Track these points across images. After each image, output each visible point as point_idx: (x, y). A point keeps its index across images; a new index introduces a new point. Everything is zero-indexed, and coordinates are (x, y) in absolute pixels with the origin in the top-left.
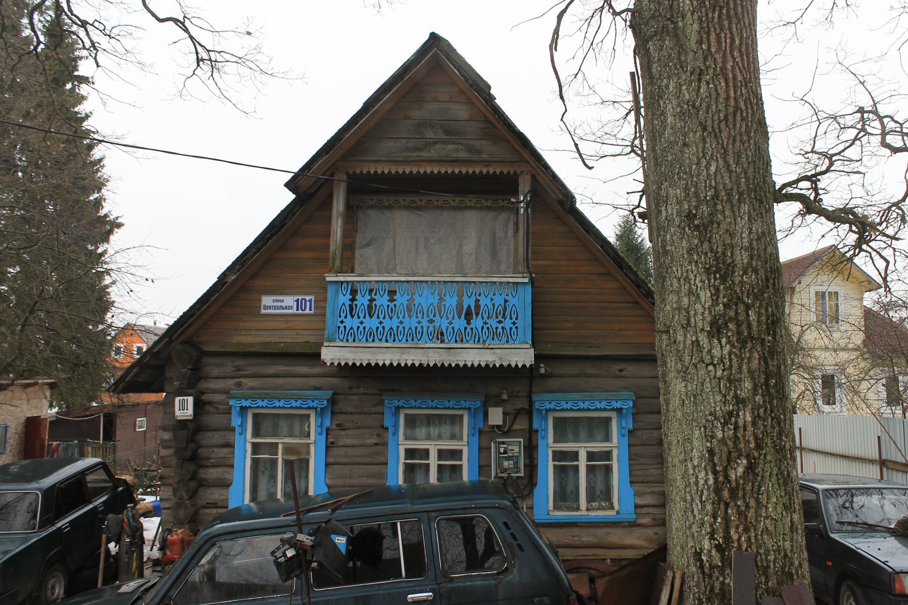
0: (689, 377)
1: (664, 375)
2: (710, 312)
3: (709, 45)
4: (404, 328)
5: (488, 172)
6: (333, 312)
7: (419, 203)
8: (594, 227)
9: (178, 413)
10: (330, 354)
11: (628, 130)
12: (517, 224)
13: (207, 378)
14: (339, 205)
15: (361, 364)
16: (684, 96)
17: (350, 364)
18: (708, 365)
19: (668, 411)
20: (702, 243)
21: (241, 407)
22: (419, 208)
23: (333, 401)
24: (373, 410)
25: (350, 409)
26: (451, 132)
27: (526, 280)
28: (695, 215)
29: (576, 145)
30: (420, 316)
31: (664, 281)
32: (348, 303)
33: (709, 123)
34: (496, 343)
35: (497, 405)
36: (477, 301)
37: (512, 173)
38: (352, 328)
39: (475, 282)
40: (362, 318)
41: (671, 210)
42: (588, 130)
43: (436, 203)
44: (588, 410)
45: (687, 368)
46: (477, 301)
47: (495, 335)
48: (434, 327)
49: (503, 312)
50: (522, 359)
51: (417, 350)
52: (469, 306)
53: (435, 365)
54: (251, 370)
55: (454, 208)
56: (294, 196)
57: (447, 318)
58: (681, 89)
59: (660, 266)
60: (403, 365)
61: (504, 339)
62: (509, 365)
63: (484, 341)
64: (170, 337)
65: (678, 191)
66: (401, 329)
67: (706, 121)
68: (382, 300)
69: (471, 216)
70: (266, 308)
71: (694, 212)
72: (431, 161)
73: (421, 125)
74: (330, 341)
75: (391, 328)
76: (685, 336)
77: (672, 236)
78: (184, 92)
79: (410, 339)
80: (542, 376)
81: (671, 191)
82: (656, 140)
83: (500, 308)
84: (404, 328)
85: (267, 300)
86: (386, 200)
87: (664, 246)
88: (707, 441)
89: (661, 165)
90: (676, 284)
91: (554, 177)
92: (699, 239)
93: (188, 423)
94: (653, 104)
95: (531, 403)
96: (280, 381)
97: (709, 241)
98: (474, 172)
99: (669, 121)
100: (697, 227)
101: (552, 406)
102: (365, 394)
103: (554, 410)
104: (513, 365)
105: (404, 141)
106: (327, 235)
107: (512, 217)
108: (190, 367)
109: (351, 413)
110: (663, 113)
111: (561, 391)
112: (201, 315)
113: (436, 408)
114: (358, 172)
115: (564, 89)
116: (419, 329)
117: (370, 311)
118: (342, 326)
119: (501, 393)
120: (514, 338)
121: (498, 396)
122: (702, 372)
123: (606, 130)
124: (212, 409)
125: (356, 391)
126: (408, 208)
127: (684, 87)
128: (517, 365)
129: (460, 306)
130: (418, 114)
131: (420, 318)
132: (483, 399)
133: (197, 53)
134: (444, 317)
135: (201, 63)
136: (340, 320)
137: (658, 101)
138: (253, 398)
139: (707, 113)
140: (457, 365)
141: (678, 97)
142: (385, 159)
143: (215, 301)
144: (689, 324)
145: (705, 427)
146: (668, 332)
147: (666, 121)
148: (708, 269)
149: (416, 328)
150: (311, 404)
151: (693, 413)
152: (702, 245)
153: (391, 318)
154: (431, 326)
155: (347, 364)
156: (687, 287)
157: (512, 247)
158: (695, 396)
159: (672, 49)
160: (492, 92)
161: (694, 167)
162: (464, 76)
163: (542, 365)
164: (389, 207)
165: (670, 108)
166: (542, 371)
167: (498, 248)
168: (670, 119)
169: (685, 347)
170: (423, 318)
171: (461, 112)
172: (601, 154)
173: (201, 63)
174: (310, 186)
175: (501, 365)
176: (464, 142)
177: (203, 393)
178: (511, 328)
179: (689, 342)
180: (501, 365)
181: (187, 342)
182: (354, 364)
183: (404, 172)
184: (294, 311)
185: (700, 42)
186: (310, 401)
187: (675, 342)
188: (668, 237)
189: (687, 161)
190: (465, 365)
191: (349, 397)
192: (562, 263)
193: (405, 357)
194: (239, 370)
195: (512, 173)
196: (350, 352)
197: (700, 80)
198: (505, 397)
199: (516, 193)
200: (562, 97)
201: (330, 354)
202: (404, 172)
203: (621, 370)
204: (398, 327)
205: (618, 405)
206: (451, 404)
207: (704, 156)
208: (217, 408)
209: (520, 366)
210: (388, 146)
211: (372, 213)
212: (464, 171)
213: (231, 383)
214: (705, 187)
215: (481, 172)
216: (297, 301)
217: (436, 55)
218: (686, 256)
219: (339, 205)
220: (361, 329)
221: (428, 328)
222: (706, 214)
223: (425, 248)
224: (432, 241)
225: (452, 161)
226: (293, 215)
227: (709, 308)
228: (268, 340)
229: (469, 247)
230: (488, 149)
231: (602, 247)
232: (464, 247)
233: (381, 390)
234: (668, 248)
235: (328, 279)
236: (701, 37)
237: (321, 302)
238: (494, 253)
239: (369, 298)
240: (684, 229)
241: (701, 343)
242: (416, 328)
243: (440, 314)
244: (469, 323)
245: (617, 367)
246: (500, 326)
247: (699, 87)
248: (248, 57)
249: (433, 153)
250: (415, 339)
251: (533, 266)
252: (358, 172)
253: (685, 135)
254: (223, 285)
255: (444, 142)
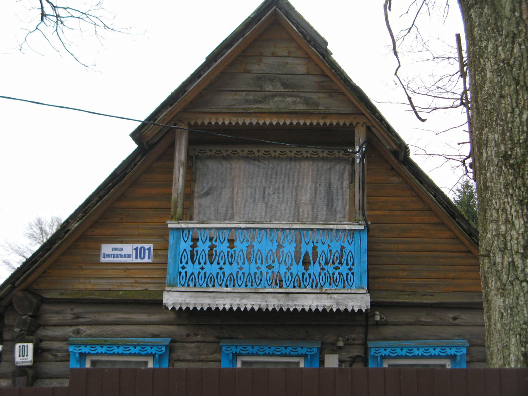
0: (507, 292)
1: (487, 295)
2: (523, 237)
3: (521, 13)
4: (243, 273)
5: (325, 124)
6: (175, 258)
7: (257, 154)
8: (427, 177)
9: (18, 359)
10: (171, 299)
11: (458, 85)
12: (352, 175)
13: (45, 326)
14: (180, 155)
15: (202, 309)
16: (500, 55)
17: (191, 308)
18: (522, 282)
19: (490, 325)
20: (516, 179)
21: (81, 354)
22: (256, 159)
23: (171, 349)
24: (210, 357)
25: (188, 357)
26: (289, 86)
27: (362, 227)
28: (510, 156)
29: (409, 98)
30: (259, 262)
31: (485, 213)
32: (189, 249)
33: (521, 78)
34: (333, 288)
35: (333, 352)
36: (315, 248)
37: (348, 124)
38: (192, 274)
39: (312, 230)
40: (202, 264)
41: (490, 152)
42: (420, 84)
43: (273, 154)
44: (422, 357)
45: (505, 285)
46: (315, 248)
47: (332, 280)
48: (273, 273)
49: (340, 259)
50: (359, 304)
51: (256, 295)
52: (307, 254)
53: (274, 309)
54: (91, 317)
55: (290, 159)
56: (137, 146)
57: (286, 264)
58: (497, 50)
59: (483, 201)
60: (242, 309)
61: (341, 285)
62: (346, 310)
63: (322, 287)
64: (13, 284)
65: (496, 136)
66: (240, 274)
67: (519, 77)
68: (223, 247)
69: (307, 167)
70: (106, 256)
71: (509, 153)
72: (270, 113)
73: (261, 78)
74: (172, 286)
75: (231, 274)
76: (503, 258)
77: (492, 174)
78: (25, 46)
79: (249, 284)
80: (377, 324)
81: (491, 136)
82: (477, 93)
83: (337, 254)
84: (243, 273)
85: (106, 249)
86: (226, 150)
87: (485, 183)
88: (522, 346)
89: (482, 114)
90: (495, 215)
91: (389, 128)
92: (514, 176)
93: (28, 370)
94: (475, 61)
95: (366, 350)
96: (118, 329)
97: (522, 178)
98: (311, 124)
99: (488, 76)
100: (512, 166)
101: (387, 352)
102: (203, 342)
103: (389, 357)
104: (350, 309)
105: (245, 93)
106: (169, 184)
107: (347, 168)
108: (30, 314)
109: (189, 361)
110: (483, 70)
111: (395, 338)
112: (44, 261)
113: (273, 355)
114: (199, 123)
115: (397, 44)
116: (258, 274)
117: (211, 256)
118: (183, 272)
119: (337, 341)
120: (351, 283)
121: (334, 344)
122: (517, 288)
123: (440, 84)
124: (50, 357)
125: (194, 339)
126: (246, 158)
127: (500, 48)
128: (353, 310)
129: (297, 253)
130: (255, 68)
131: (259, 264)
132: (319, 346)
133: (42, 8)
134: (283, 264)
135: (45, 18)
136: (181, 265)
137: (479, 59)
138: (93, 345)
139: (520, 70)
140: (295, 310)
141: (496, 56)
142: (226, 110)
143: (57, 248)
144: (506, 248)
145: (520, 335)
146: (489, 256)
147: (486, 76)
148: (521, 201)
149: (255, 273)
150: (150, 351)
151: (510, 323)
152: (516, 181)
153: (231, 264)
154: (270, 272)
155: (188, 308)
156: (504, 217)
157: (347, 197)
158: (511, 309)
159: (489, 16)
160: (329, 47)
161: (509, 115)
162: (302, 33)
163: (377, 313)
164: (226, 158)
165: (489, 65)
166: (378, 318)
167: (334, 198)
168: (489, 75)
169: (503, 268)
170: (262, 263)
171: (299, 66)
172: (433, 106)
173: (45, 18)
174: (154, 137)
175: (338, 310)
176: (301, 94)
177: (41, 341)
178: (347, 274)
179: (506, 263)
180: (338, 310)
181: (26, 290)
182: (195, 308)
183: (244, 123)
184: (134, 259)
185: (513, 11)
186: (148, 348)
187: (495, 264)
188: (488, 174)
189: (504, 110)
190: (303, 310)
191: (186, 344)
192: (397, 213)
193: (245, 301)
194: (78, 317)
195: (348, 124)
196: (191, 297)
197: (513, 43)
198: (341, 344)
199: (352, 145)
200: (395, 53)
201: (171, 299)
202: (244, 123)
203: (455, 319)
204: (238, 272)
205: (452, 352)
206: (288, 351)
207: (517, 106)
208: (56, 356)
209: (356, 310)
210: (227, 99)
211: (211, 164)
212: (302, 122)
213: (69, 330)
214: (519, 132)
215: (318, 124)
216: (136, 249)
217: (275, 13)
218: (503, 190)
219: (180, 155)
220: (202, 274)
221: (267, 273)
222: (519, 154)
223: (262, 198)
224: (269, 191)
225: (291, 113)
226: (135, 165)
227: (522, 234)
228: (106, 287)
229: (305, 197)
230: (325, 102)
231: (435, 196)
232: (301, 197)
233: (218, 338)
234: (489, 184)
235: (170, 226)
236: (514, 6)
237: (162, 249)
238: (330, 204)
239: (210, 244)
240: (501, 168)
241: (516, 263)
242: (255, 273)
243: (278, 261)
244: (306, 269)
245: (451, 315)
246: (337, 272)
247: (513, 48)
248: (90, 13)
249: (272, 105)
250: (255, 285)
251: (369, 216)
252: (199, 123)
253: (502, 88)
254: (66, 232)
255: (282, 95)
